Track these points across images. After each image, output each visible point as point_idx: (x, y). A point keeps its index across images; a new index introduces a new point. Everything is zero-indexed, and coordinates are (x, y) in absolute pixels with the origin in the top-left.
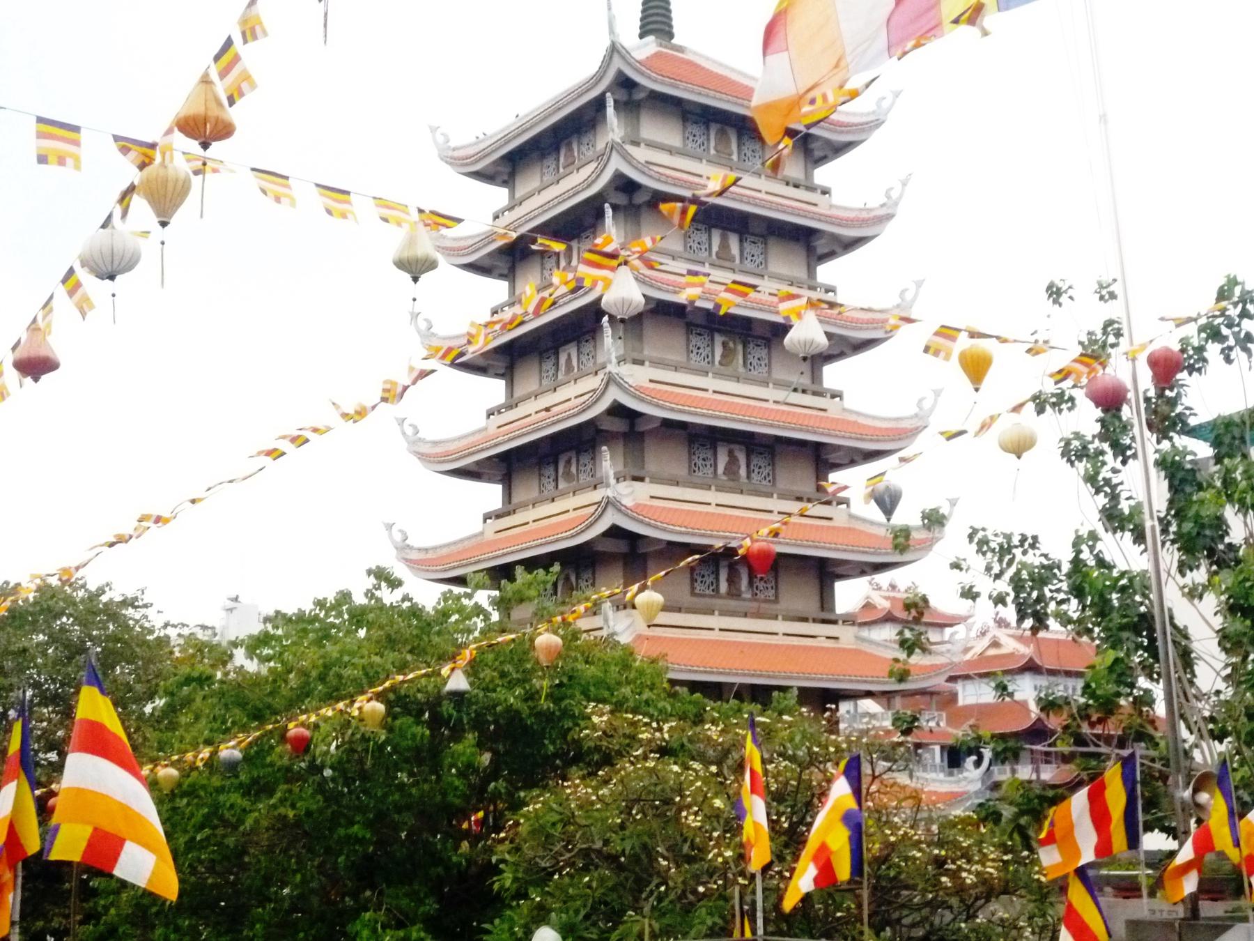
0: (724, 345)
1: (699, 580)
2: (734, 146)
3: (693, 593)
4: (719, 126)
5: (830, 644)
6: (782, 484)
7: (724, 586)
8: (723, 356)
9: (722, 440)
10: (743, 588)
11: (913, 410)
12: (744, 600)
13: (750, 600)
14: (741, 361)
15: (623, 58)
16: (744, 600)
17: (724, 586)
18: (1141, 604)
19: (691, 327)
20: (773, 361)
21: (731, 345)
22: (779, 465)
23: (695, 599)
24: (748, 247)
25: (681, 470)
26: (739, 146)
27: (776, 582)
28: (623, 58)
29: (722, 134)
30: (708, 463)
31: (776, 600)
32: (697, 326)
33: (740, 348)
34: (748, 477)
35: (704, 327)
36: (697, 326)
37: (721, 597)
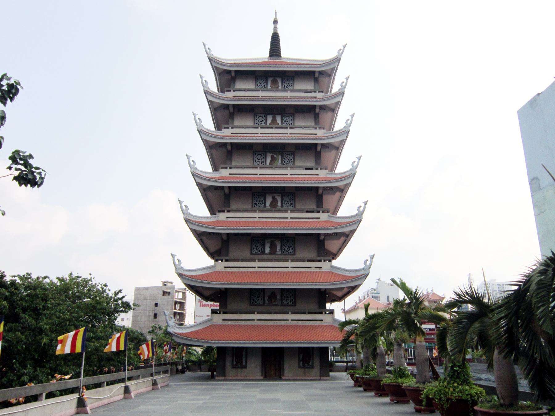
0: (272, 157)
1: (255, 248)
2: (280, 84)
3: (251, 254)
4: (272, 78)
5: (318, 270)
6: (298, 206)
7: (267, 250)
8: (271, 161)
9: (268, 193)
10: (278, 250)
11: (362, 266)
12: (277, 255)
13: (280, 255)
14: (280, 161)
15: (214, 61)
16: (277, 255)
17: (267, 250)
18: (453, 383)
19: (255, 153)
20: (296, 250)
21: (275, 156)
22: (296, 158)
23: (252, 256)
24: (285, 119)
25: (250, 164)
26: (282, 85)
27: (294, 160)
28: (214, 61)
29: (275, 82)
30: (261, 203)
31: (294, 254)
32: (259, 151)
33: (280, 157)
34: (282, 206)
35: (262, 114)
36: (259, 151)
37: (267, 254)
